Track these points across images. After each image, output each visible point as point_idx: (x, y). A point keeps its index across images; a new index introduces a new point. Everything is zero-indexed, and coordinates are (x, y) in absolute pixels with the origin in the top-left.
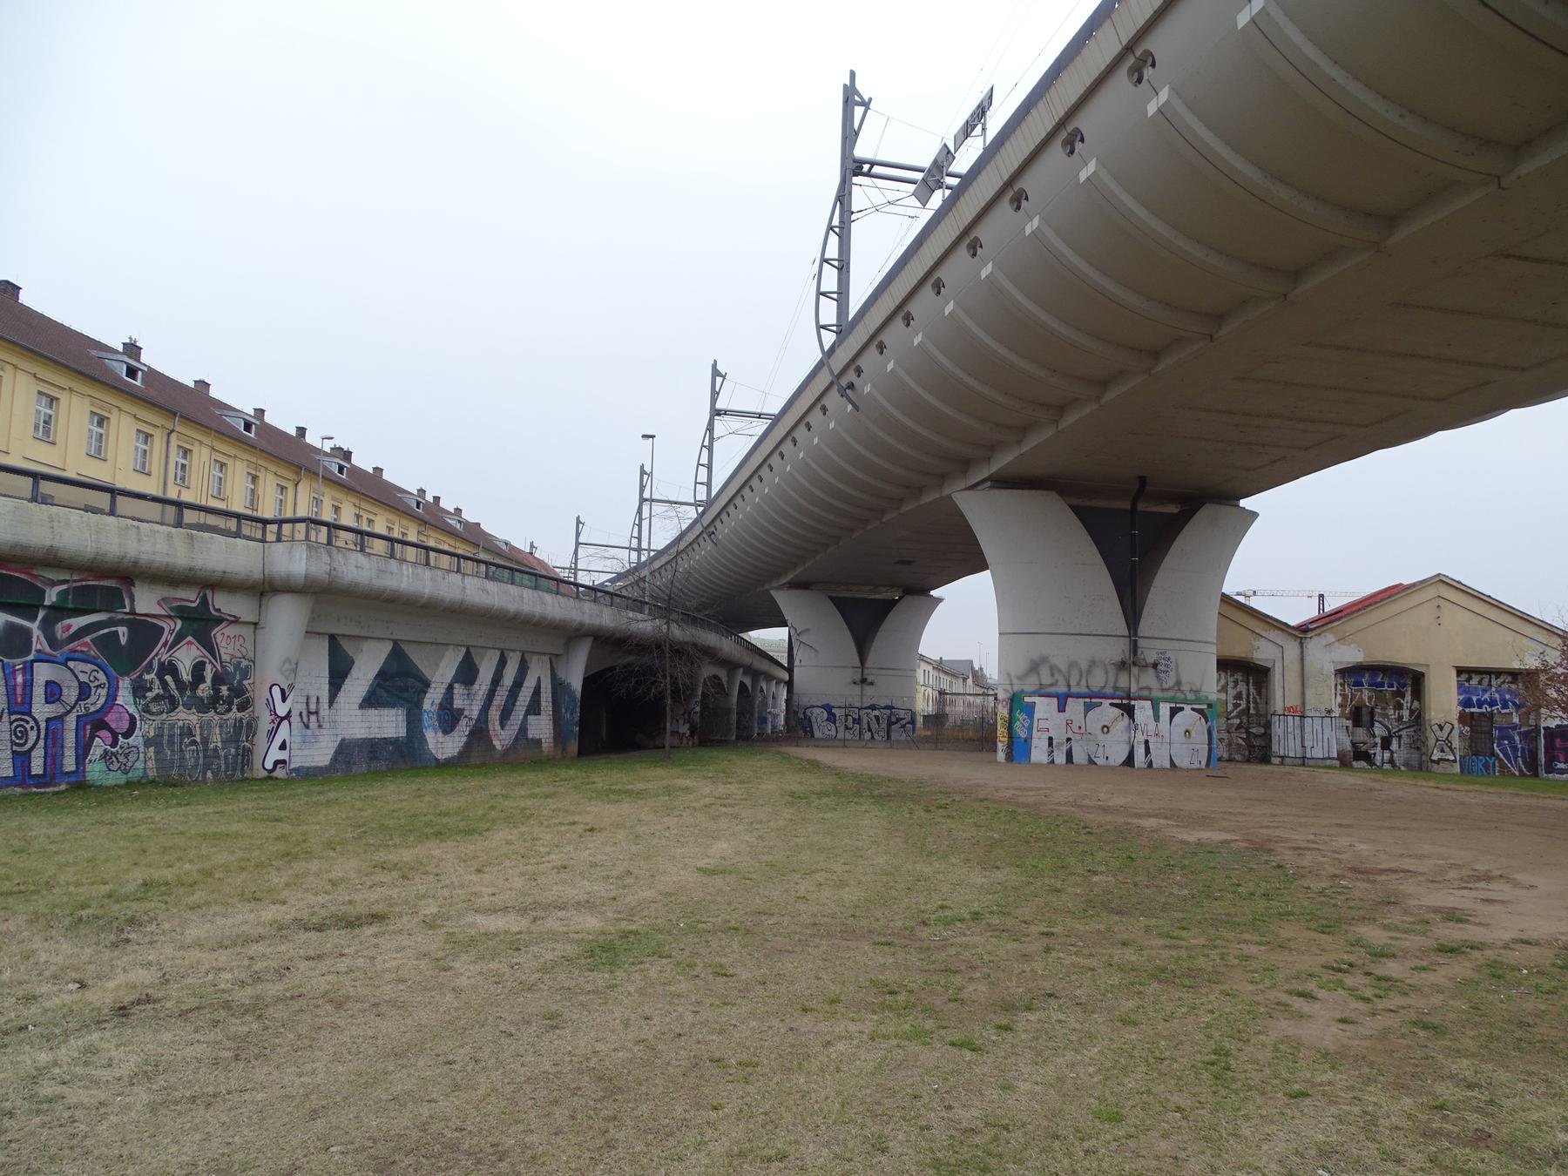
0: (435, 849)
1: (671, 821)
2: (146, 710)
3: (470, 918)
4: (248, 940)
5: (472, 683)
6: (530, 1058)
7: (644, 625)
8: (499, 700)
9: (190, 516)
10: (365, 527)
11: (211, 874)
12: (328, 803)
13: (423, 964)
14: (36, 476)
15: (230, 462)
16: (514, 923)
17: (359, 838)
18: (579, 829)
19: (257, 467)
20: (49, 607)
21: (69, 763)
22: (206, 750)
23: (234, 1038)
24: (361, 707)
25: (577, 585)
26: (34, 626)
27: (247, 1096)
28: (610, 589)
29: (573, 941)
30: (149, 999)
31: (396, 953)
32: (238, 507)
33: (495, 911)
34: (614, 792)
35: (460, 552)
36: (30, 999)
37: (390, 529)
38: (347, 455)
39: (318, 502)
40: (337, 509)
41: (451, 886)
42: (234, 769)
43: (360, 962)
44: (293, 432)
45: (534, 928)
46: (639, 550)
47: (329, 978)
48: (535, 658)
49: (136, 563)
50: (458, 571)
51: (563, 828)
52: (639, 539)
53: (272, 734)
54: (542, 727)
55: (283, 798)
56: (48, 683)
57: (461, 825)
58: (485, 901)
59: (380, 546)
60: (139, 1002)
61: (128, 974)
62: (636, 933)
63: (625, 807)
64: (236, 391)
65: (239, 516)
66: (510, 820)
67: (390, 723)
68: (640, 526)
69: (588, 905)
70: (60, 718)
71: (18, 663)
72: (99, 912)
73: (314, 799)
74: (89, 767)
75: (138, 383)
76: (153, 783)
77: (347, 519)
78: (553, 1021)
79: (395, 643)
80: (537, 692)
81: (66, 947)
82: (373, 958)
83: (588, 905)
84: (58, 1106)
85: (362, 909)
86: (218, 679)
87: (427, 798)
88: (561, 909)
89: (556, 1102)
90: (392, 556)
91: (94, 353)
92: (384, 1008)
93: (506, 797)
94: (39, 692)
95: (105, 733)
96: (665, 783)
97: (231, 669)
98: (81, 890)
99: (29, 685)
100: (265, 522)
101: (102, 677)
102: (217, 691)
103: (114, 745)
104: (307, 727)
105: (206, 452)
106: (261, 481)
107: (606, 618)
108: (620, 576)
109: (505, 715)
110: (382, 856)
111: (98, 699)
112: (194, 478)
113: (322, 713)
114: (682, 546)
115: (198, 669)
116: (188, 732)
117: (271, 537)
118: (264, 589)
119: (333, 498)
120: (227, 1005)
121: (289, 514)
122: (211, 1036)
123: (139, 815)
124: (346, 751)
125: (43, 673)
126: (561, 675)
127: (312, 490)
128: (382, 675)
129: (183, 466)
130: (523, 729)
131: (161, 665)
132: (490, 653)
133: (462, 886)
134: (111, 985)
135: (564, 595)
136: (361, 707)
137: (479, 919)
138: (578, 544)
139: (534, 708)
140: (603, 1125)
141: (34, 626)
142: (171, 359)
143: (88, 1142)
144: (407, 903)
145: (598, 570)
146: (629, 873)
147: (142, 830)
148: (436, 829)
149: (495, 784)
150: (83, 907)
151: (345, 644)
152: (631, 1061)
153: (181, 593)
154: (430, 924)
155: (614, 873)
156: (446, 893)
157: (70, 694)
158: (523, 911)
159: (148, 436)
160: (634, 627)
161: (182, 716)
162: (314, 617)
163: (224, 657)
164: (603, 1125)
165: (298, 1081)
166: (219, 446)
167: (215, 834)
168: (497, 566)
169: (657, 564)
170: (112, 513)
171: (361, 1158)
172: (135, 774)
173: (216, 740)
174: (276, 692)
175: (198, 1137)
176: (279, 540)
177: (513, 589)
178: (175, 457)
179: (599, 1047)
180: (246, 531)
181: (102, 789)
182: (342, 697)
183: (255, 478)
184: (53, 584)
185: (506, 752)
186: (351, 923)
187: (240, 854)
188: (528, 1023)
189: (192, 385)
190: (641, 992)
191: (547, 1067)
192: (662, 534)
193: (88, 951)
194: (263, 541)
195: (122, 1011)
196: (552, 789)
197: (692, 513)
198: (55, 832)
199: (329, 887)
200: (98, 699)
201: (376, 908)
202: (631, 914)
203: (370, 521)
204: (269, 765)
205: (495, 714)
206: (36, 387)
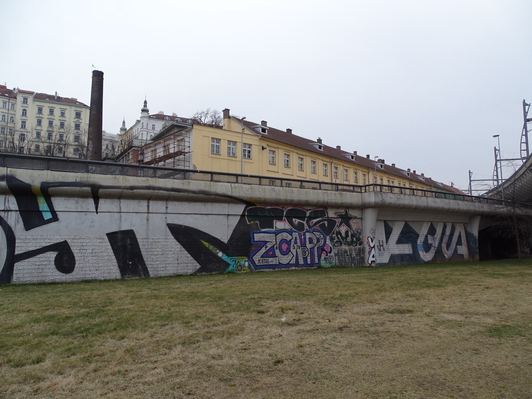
0: (427, 291)
1: (524, 287)
2: (334, 245)
3: (442, 314)
4: (371, 314)
5: (434, 234)
6: (468, 362)
7: (503, 209)
8: (445, 240)
9: (340, 187)
10: (391, 184)
11: (358, 294)
12: (389, 275)
13: (427, 327)
14: (212, 173)
15: (276, 150)
16: (459, 318)
17: (401, 286)
18: (482, 287)
19: (356, 170)
20: (308, 217)
21: (316, 261)
22: (351, 257)
23: (371, 340)
24: (397, 243)
25: (472, 197)
26: (305, 222)
27: (377, 357)
28: (486, 197)
29: (482, 326)
30: (347, 327)
31: (418, 323)
32: (352, 183)
33: (451, 313)
34: (496, 274)
35: (425, 189)
36: (318, 323)
37: (399, 184)
38: (383, 161)
39: (375, 178)
40: (382, 179)
41: (434, 304)
42: (359, 263)
43: (406, 324)
44: (366, 157)
45: (466, 320)
46: (497, 180)
47: (397, 328)
48: (458, 225)
49: (327, 203)
50: (425, 196)
51: (475, 287)
52: (497, 176)
53: (370, 252)
54: (463, 250)
55: (375, 273)
56: (309, 238)
57: (436, 284)
58: (447, 309)
59: (396, 190)
60: (344, 327)
61: (340, 320)
62: (509, 326)
63: (501, 280)
64: (348, 148)
65: (353, 186)
66: (454, 283)
67: (406, 249)
68: (497, 171)
69: (487, 314)
70: (313, 248)
71: (302, 233)
72: (330, 302)
73: (385, 273)
74: (321, 262)
75: (322, 150)
76: (338, 267)
77: (385, 183)
78: (476, 352)
79: (406, 222)
80: (460, 237)
81: (324, 310)
82: (409, 324)
83: (487, 314)
84: (329, 350)
85: (404, 308)
86: (353, 236)
87: (422, 274)
88: (476, 315)
89: (480, 378)
90: (402, 193)
91: (310, 144)
92: (415, 339)
93: (451, 275)
94: (307, 240)
95: (324, 252)
96: (519, 271)
97: (356, 232)
98: (325, 295)
99: (305, 238)
100: (361, 187)
101: (322, 236)
102: (352, 239)
103: (327, 255)
104: (380, 250)
105: (342, 167)
106: (358, 174)
107: (485, 208)
108: (490, 191)
109: (448, 246)
110: (409, 292)
111: (322, 242)
112: (339, 176)
113: (384, 246)
114: (517, 177)
115: (347, 233)
116: (346, 252)
117: (363, 191)
118: (363, 207)
119: (380, 176)
120: (368, 331)
121: (367, 184)
122: (365, 339)
123: (336, 276)
124: (393, 258)
125: (308, 235)
126: (469, 230)
127: (373, 174)
128: (402, 233)
129: (288, 161)
130: (456, 250)
131: (337, 232)
132: (440, 224)
133: (438, 304)
134: (336, 322)
135: (467, 201)
136: (397, 243)
137: (445, 315)
138: (471, 181)
139: (459, 243)
140: (500, 389)
141: (305, 222)
142: (330, 142)
143: (337, 361)
144: (419, 308)
145: (480, 189)
146: (505, 304)
147: (337, 280)
148: (427, 284)
149: (447, 270)
150: (326, 300)
151: (389, 223)
152: (509, 370)
153: (340, 211)
154: (428, 315)
155: (498, 304)
156: (432, 306)
157: (315, 241)
158: (462, 314)
159: (326, 165)
160: (498, 210)
161: (344, 247)
162: (379, 215)
163: (354, 229)
164: (500, 389)
165: (391, 356)
166: (300, 152)
167: (357, 283)
168: (439, 193)
169: (506, 185)
170: (320, 189)
171: (413, 381)
172: (333, 264)
173: (354, 254)
174: (370, 239)
175: (365, 365)
176: (366, 192)
177: (446, 201)
178: (334, 170)
179: (495, 363)
180: (355, 190)
181: (325, 268)
182: (390, 240)
183: (356, 173)
184: (308, 210)
185: (450, 259)
186: (402, 312)
187: (365, 289)
188: (467, 351)
189: (336, 148)
190: (512, 347)
191: (475, 366)
192: (507, 172)
193: (329, 312)
194: (361, 192)
195: (341, 329)
196: (469, 272)
197: (521, 163)
198: (316, 279)
199: (393, 301)
200: (322, 242)
201: (410, 308)
202: (507, 319)
203: (393, 182)
204: (370, 262)
205: (444, 246)
206: (298, 156)
